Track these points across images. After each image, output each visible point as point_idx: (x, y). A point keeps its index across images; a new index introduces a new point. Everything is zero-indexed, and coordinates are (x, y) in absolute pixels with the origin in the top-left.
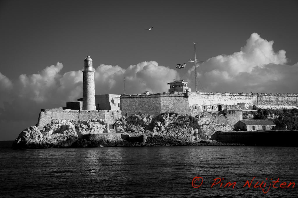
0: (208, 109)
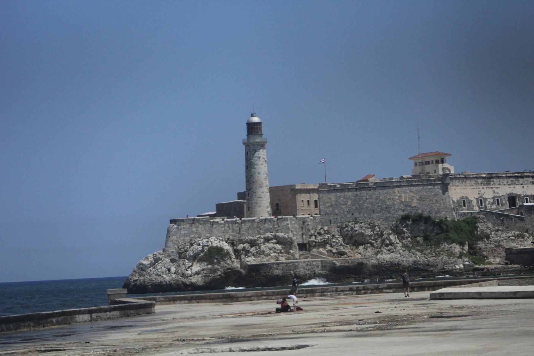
0: (489, 205)
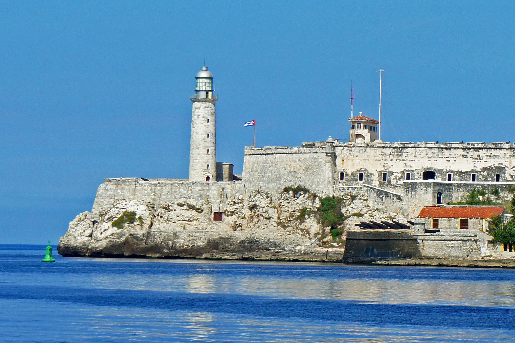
0: (395, 180)
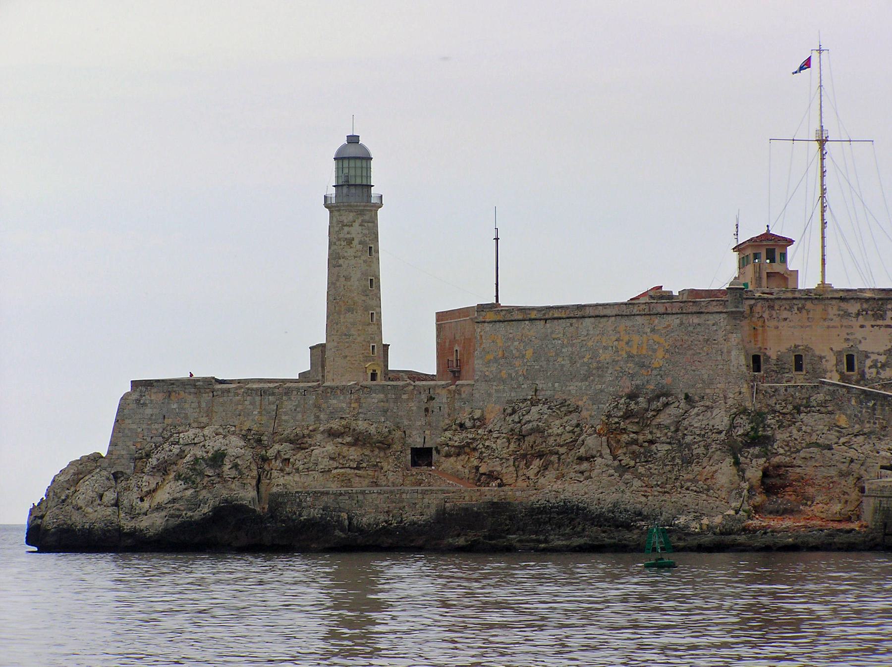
0: (874, 370)
